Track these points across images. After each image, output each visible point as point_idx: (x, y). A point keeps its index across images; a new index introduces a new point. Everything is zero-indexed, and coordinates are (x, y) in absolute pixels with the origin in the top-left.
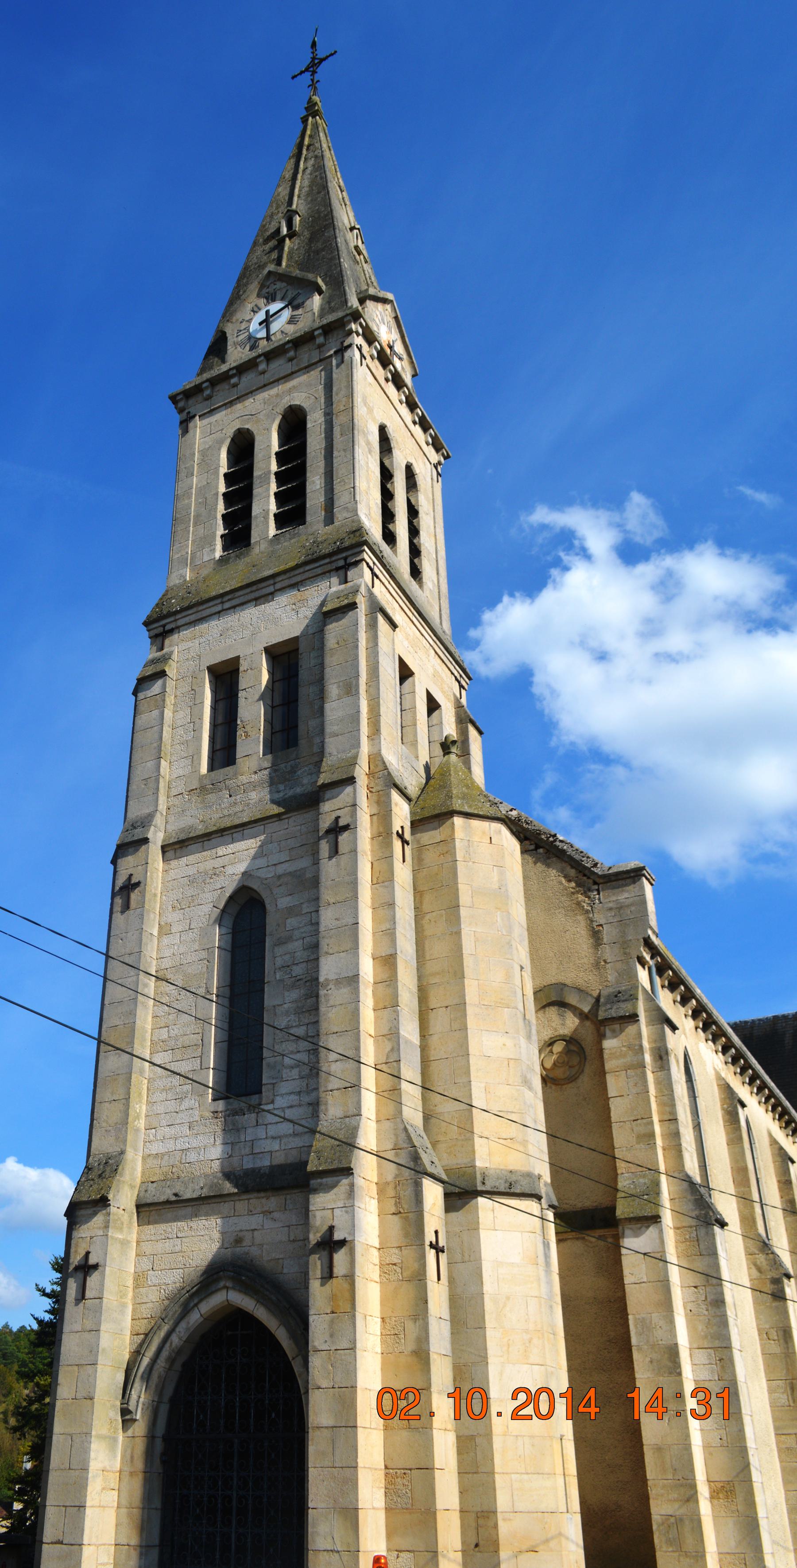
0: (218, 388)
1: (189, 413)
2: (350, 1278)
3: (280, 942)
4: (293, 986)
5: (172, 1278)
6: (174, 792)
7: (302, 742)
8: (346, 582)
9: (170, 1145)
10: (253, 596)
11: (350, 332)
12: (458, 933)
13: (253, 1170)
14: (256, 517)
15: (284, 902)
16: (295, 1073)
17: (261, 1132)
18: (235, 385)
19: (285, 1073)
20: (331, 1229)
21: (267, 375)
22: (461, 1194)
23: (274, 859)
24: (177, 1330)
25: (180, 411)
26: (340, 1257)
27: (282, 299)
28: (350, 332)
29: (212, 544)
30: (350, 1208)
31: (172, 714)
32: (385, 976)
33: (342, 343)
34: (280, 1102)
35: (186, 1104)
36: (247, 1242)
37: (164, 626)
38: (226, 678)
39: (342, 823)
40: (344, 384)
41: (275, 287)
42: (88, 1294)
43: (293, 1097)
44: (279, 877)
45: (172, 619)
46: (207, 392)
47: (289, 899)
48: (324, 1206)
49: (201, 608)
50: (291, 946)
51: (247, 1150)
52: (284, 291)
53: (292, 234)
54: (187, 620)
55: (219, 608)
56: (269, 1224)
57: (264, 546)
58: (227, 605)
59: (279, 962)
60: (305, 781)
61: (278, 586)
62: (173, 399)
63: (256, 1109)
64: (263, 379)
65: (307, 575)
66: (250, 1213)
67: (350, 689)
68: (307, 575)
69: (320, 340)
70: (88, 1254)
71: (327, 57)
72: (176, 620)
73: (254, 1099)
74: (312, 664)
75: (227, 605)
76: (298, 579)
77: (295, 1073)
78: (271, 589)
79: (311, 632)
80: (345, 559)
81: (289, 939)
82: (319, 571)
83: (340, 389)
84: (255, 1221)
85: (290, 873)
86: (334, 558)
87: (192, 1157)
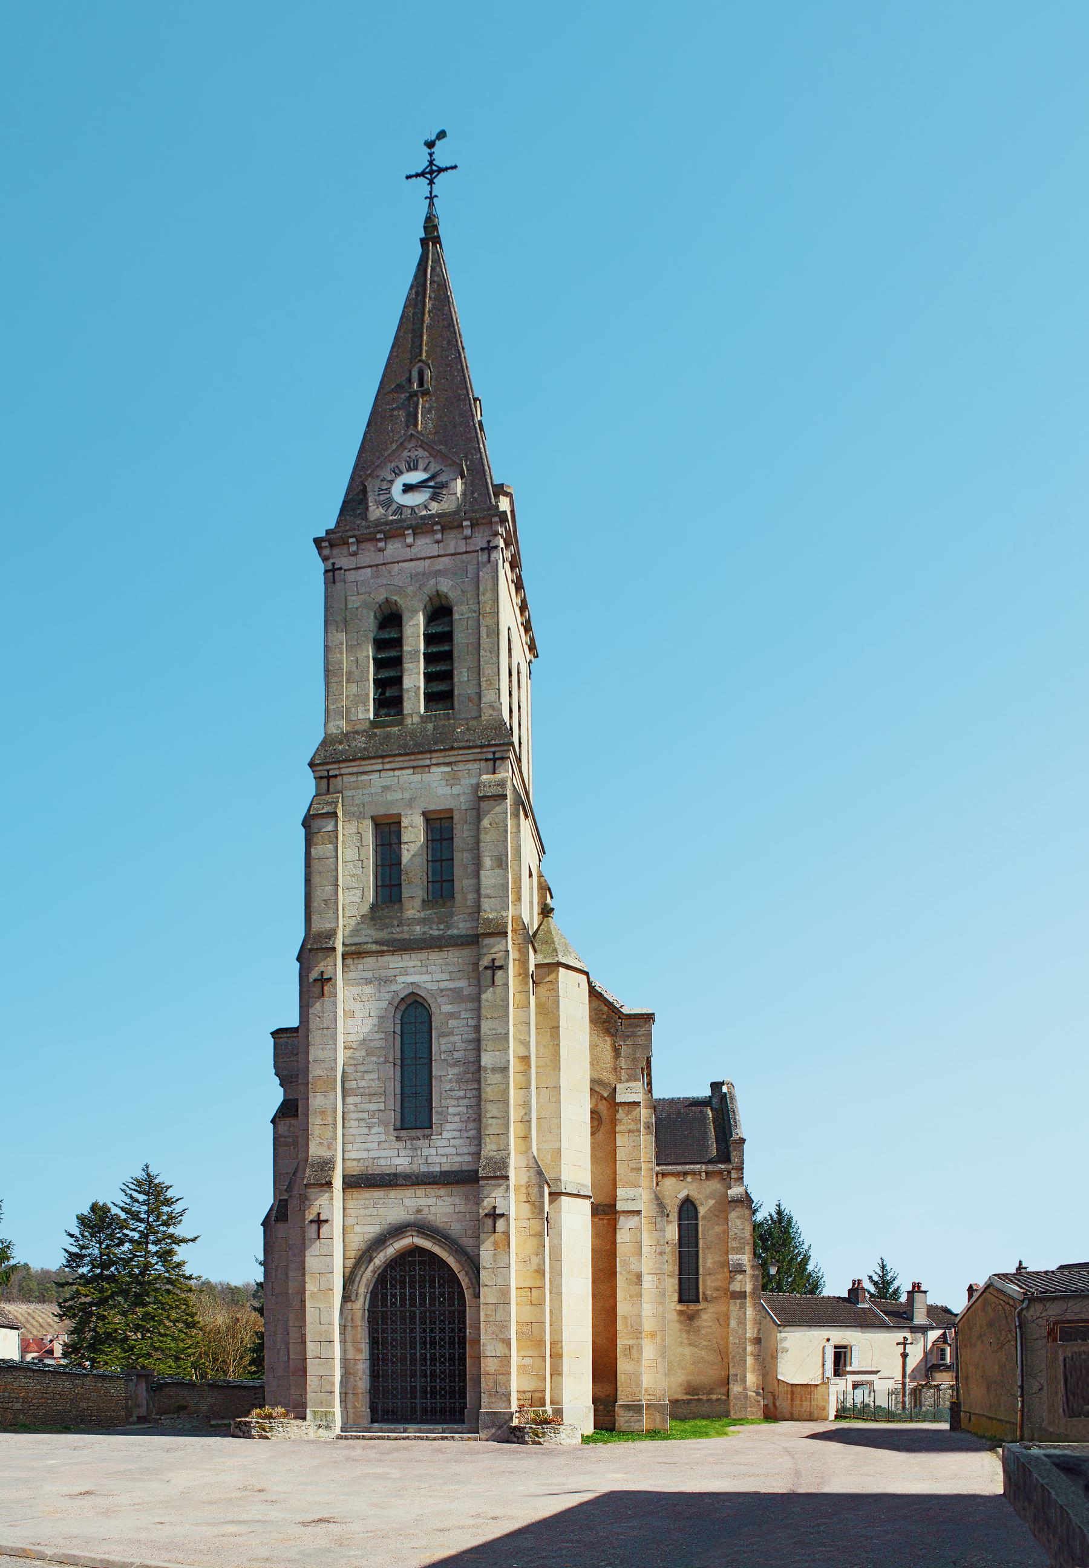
0: (363, 546)
1: (333, 564)
2: (507, 1234)
3: (443, 1035)
4: (454, 1065)
5: (366, 1231)
6: (348, 914)
7: (458, 896)
8: (494, 773)
9: (364, 1155)
10: (412, 764)
11: (496, 534)
12: (558, 1045)
13: (428, 1173)
14: (408, 690)
15: (447, 1008)
16: (457, 1118)
17: (433, 1151)
18: (381, 550)
19: (450, 1118)
20: (495, 1208)
21: (414, 550)
22: (555, 1195)
23: (438, 977)
24: (1071, 1303)
25: (325, 559)
26: (500, 1223)
27: (425, 470)
28: (496, 534)
29: (365, 703)
30: (507, 1198)
31: (347, 852)
32: (521, 1069)
33: (489, 542)
34: (445, 1135)
35: (374, 1130)
36: (426, 1211)
37: (328, 771)
38: (387, 831)
39: (497, 964)
40: (490, 585)
41: (416, 453)
42: (321, 1236)
43: (455, 1133)
44: (442, 990)
45: (336, 766)
46: (353, 548)
47: (450, 1006)
48: (493, 1198)
49: (363, 763)
50: (452, 1039)
51: (423, 1161)
52: (427, 461)
53: (426, 393)
54: (350, 770)
55: (380, 767)
56: (440, 1203)
57: (416, 719)
58: (387, 766)
59: (443, 1048)
60: (461, 925)
61: (434, 761)
62: (317, 542)
63: (428, 1137)
64: (409, 553)
65: (459, 758)
66: (426, 1196)
67: (501, 863)
68: (459, 758)
69: (468, 532)
70: (319, 1214)
71: (446, 169)
72: (340, 768)
73: (427, 1131)
74: (465, 835)
75: (387, 766)
76: (453, 759)
77: (457, 1118)
78: (428, 762)
79: (464, 807)
80: (494, 753)
81: (452, 1033)
82: (471, 757)
83: (486, 590)
84: (431, 1201)
85: (450, 989)
86: (485, 750)
87: (382, 1162)
